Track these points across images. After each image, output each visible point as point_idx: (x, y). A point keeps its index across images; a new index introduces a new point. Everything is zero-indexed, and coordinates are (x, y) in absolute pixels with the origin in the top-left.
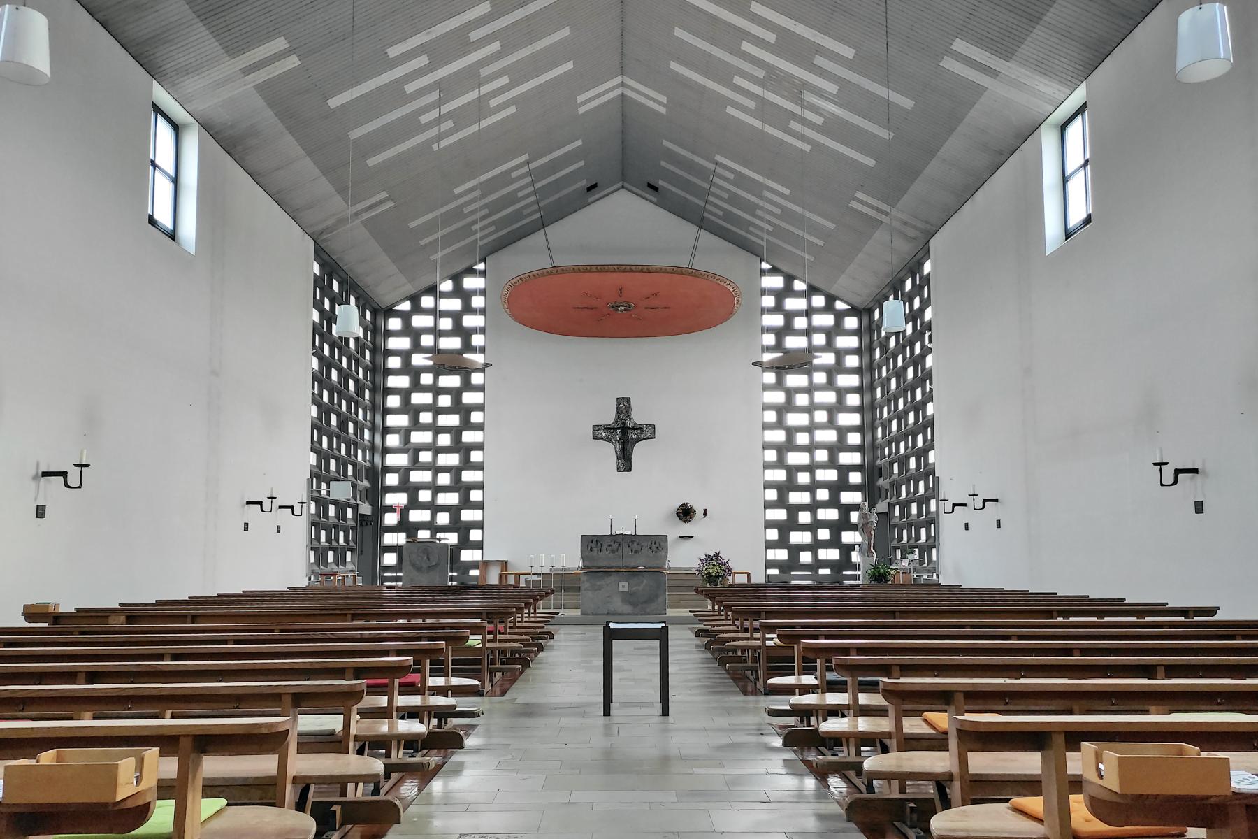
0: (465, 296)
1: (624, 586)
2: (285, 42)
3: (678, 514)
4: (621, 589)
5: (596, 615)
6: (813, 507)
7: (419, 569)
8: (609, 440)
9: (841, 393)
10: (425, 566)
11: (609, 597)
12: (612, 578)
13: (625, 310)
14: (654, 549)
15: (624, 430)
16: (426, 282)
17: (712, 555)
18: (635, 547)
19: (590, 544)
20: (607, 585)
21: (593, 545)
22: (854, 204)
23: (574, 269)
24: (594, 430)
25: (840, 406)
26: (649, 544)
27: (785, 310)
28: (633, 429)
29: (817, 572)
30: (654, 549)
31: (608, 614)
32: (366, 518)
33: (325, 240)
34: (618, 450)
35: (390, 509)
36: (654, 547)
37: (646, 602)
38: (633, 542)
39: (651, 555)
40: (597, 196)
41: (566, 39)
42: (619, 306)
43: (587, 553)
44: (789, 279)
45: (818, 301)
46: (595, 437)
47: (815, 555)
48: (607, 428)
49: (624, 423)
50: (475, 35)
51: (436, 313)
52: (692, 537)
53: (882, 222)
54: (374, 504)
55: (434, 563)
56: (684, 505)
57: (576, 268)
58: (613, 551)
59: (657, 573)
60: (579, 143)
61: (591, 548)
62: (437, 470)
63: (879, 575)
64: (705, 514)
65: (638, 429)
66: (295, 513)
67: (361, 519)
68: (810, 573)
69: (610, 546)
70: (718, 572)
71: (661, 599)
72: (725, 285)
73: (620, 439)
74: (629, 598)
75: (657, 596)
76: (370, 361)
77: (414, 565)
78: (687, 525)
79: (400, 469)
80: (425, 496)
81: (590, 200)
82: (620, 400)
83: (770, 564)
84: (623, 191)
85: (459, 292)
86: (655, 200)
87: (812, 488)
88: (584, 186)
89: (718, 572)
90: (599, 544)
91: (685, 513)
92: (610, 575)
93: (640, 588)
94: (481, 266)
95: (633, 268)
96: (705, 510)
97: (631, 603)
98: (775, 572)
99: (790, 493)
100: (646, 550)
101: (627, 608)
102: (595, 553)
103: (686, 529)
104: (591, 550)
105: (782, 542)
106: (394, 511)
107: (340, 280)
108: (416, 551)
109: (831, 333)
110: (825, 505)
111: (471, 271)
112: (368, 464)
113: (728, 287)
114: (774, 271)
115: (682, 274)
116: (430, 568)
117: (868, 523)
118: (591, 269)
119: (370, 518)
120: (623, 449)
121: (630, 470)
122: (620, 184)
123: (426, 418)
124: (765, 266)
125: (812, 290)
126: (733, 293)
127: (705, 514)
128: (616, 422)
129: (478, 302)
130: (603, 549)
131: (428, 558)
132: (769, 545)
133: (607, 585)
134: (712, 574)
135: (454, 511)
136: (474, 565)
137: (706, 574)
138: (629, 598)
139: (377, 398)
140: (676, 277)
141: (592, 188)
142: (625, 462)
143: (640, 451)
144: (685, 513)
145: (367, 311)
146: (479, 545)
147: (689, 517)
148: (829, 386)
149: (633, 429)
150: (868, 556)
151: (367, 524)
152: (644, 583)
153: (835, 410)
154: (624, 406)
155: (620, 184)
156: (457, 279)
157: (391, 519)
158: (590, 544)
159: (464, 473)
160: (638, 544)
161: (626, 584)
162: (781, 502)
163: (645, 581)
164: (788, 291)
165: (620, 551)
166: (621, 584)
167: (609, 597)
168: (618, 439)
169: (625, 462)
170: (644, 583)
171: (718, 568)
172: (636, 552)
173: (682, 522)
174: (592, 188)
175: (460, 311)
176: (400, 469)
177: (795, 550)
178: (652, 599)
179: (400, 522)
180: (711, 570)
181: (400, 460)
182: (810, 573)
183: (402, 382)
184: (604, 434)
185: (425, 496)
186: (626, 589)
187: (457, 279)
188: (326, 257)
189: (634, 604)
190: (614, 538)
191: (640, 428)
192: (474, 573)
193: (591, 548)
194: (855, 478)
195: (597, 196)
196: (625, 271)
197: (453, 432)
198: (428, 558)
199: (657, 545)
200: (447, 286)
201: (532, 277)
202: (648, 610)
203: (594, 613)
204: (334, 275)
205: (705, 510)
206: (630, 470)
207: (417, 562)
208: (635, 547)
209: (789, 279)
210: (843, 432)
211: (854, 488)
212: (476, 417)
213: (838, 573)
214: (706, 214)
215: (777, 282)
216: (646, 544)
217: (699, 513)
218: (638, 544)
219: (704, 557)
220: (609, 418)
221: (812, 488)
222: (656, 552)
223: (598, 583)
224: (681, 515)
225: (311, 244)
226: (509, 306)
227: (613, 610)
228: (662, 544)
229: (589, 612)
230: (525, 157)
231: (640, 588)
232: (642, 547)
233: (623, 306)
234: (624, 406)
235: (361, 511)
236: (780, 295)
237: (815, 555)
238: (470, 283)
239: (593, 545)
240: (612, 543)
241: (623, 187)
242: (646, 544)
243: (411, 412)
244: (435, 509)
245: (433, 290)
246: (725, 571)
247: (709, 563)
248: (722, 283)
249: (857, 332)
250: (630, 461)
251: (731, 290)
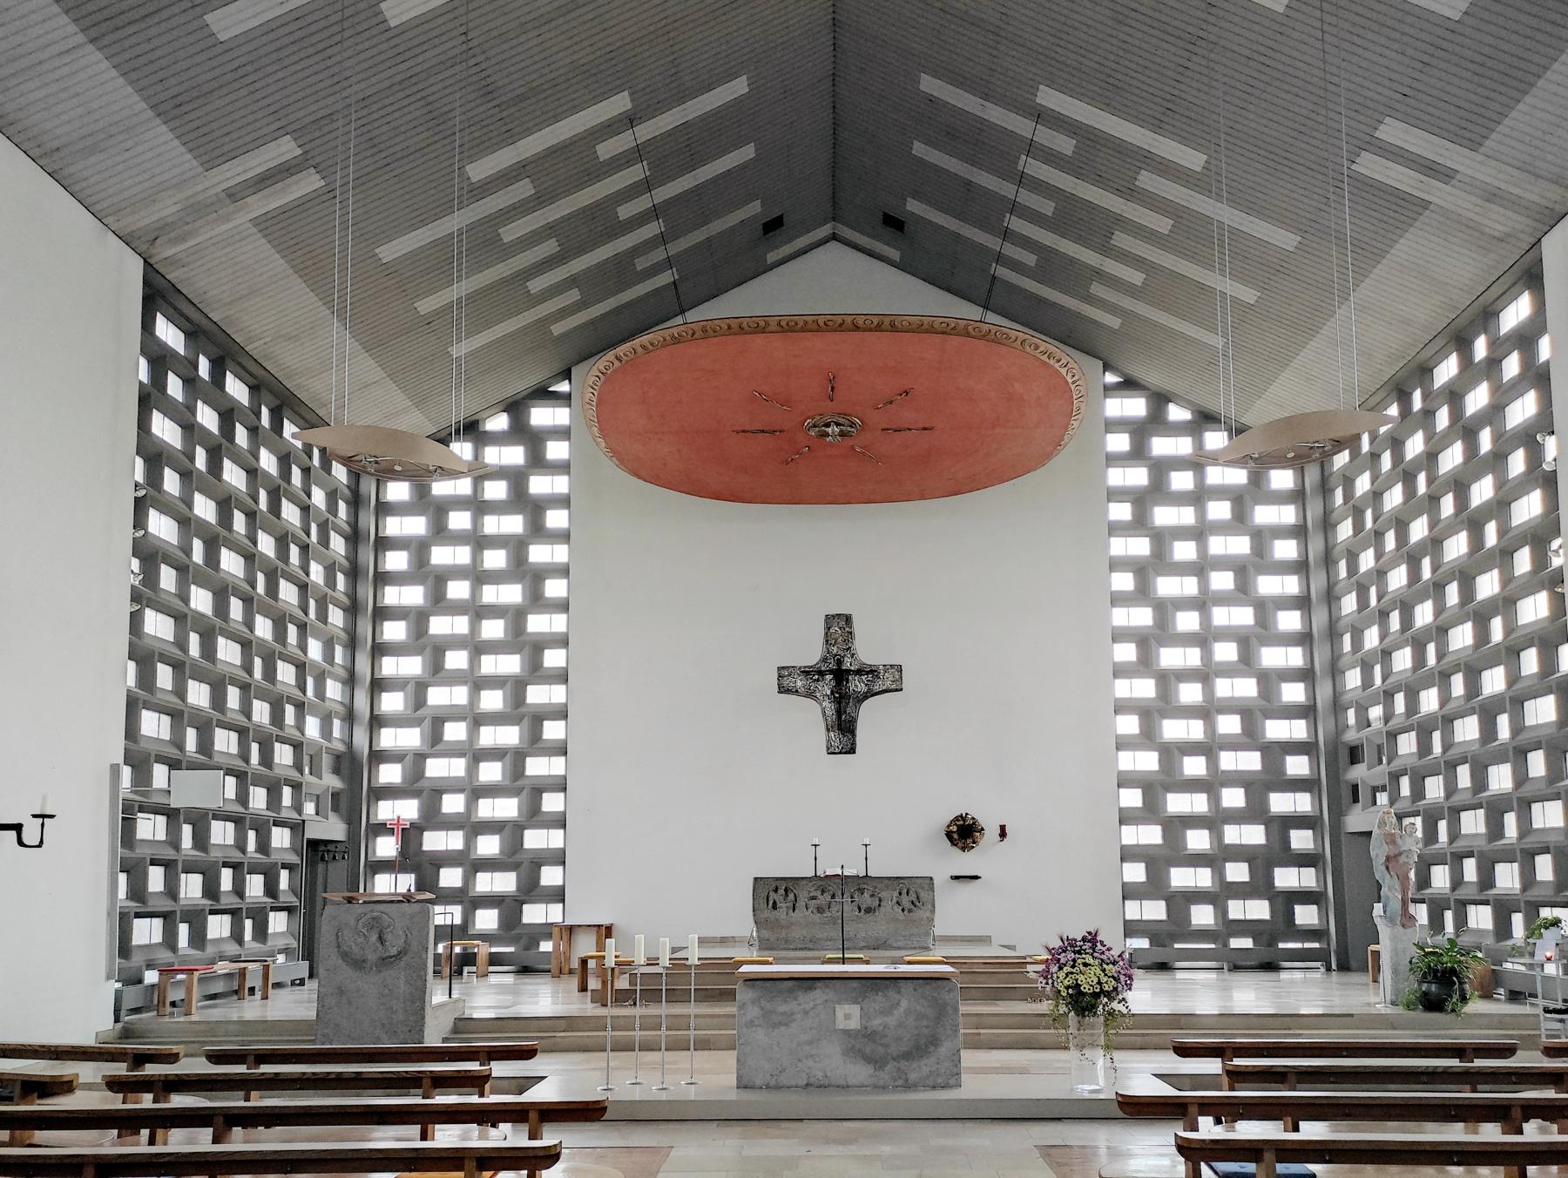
0: (534, 440)
1: (849, 1016)
2: (214, 28)
3: (949, 835)
4: (841, 1024)
5: (778, 1088)
6: (1215, 821)
7: (359, 964)
8: (810, 694)
9: (1265, 608)
10: (372, 957)
11: (810, 1043)
12: (819, 995)
13: (842, 434)
14: (907, 904)
15: (840, 675)
16: (458, 412)
17: (1079, 938)
18: (866, 900)
19: (773, 896)
20: (806, 1013)
21: (778, 897)
22: (1370, 165)
23: (729, 327)
24: (780, 676)
25: (1264, 631)
26: (896, 894)
27: (1150, 458)
28: (859, 672)
29: (1226, 945)
30: (907, 904)
31: (808, 1085)
32: (322, 848)
33: (173, 261)
34: (828, 712)
35: (382, 829)
36: (905, 901)
37: (907, 1056)
38: (861, 891)
39: (901, 916)
40: (786, 250)
41: (738, 102)
42: (828, 425)
43: (767, 913)
44: (1159, 400)
45: (1216, 440)
46: (783, 690)
47: (1222, 911)
48: (806, 672)
49: (839, 662)
50: (641, 264)
51: (481, 474)
52: (977, 878)
53: (1425, 205)
54: (352, 820)
55: (394, 951)
56: (962, 817)
57: (734, 323)
58: (820, 910)
59: (934, 984)
60: (739, 87)
61: (775, 903)
62: (478, 756)
63: (1444, 971)
64: (1003, 833)
65: (868, 673)
66: (26, 840)
67: (317, 850)
68: (1213, 946)
69: (814, 898)
70: (1099, 983)
71: (944, 1050)
72: (1057, 366)
73: (832, 693)
74: (863, 1045)
75: (934, 1041)
76: (347, 558)
77: (345, 956)
78: (968, 855)
79: (406, 755)
80: (453, 804)
81: (771, 257)
82: (830, 620)
83: (1131, 929)
84: (833, 244)
85: (521, 432)
86: (895, 254)
87: (1210, 785)
88: (755, 217)
89: (1099, 983)
90: (791, 896)
91: (964, 833)
92: (811, 988)
93: (892, 1021)
94: (564, 387)
95: (860, 320)
96: (1003, 828)
97: (868, 1060)
98: (1143, 943)
99: (1243, 790)
100: (888, 906)
101: (859, 1072)
102: (781, 914)
103: (964, 862)
104: (775, 906)
105: (1155, 887)
106: (391, 832)
107: (252, 381)
108: (352, 923)
109: (1241, 500)
110: (1237, 817)
111: (543, 394)
112: (341, 747)
113: (1064, 371)
114: (1129, 385)
115: (968, 335)
116: (386, 962)
117: (1400, 854)
118: (767, 324)
119: (341, 848)
120: (839, 713)
121: (852, 751)
122: (825, 231)
123: (456, 660)
124: (1111, 378)
125: (1205, 419)
126: (1073, 387)
127: (1003, 833)
128: (824, 660)
129: (557, 450)
130: (801, 904)
131: (381, 939)
132: (1130, 892)
133: (806, 1013)
134: (1085, 988)
135: (511, 831)
136: (546, 931)
137: (1068, 988)
138: (863, 1045)
139: (359, 623)
140: (955, 341)
141: (773, 225)
142: (844, 731)
143: (869, 716)
144: (964, 833)
145: (263, 408)
146: (558, 895)
147: (969, 841)
148: (1242, 596)
149: (859, 672)
150: (1403, 926)
151: (334, 858)
152: (901, 1010)
153: (1172, 678)
154: (839, 627)
155: (825, 231)
156: (516, 408)
157: (386, 847)
158: (773, 896)
159: (530, 761)
160: (872, 896)
161: (855, 1010)
162: (1151, 811)
163: (904, 1004)
164: (1156, 421)
165: (834, 908)
166: (841, 1010)
167: (810, 1043)
168: (829, 693)
169: (844, 731)
170: (901, 1010)
171: (1099, 971)
172: (869, 910)
173: (956, 851)
174: (773, 225)
175: (524, 466)
176: (406, 755)
177: (1181, 901)
178: (922, 1047)
179: (404, 852)
180: (1081, 978)
181: (408, 738)
182: (1213, 946)
183: (412, 595)
184: (799, 684)
185: (453, 804)
186: (854, 1024)
187: (516, 408)
188: (259, 372)
189: (877, 1062)
190: (824, 883)
191: (872, 672)
192: (546, 946)
193: (775, 903)
194: (1297, 766)
195: (786, 250)
196: (841, 327)
197: (509, 686)
198: (381, 939)
199: (913, 897)
200: (499, 423)
201: (640, 350)
202: (913, 1077)
203: (773, 1083)
204: (229, 363)
205: (1003, 828)
206: (852, 751)
207: (355, 949)
208: (866, 900)
209: (1159, 400)
210: (1269, 680)
211: (1297, 785)
212: (554, 658)
213: (1270, 945)
214: (1002, 272)
215: (1135, 407)
216: (889, 896)
217: (991, 832)
218: (872, 896)
219: (1057, 944)
220: (812, 654)
221: (1210, 785)
222: (910, 911)
223: (783, 1008)
224: (956, 836)
225: (136, 267)
226: (601, 430)
227: (820, 1075)
228: (923, 895)
229: (758, 1082)
230: (620, 103)
231: (892, 1021)
232: (880, 900)
233: (838, 424)
234: (839, 627)
235: (312, 833)
236: (1141, 431)
237: (1222, 911)
238: (542, 416)
239: (778, 897)
240: (818, 893)
241: (834, 237)
242: (889, 896)
243: (428, 651)
244: (475, 828)
245: (471, 429)
246: (1117, 980)
247: (1074, 961)
248: (1052, 362)
249: (1297, 496)
250: (852, 732)
251: (1070, 381)
